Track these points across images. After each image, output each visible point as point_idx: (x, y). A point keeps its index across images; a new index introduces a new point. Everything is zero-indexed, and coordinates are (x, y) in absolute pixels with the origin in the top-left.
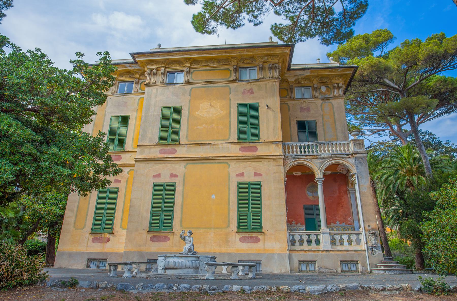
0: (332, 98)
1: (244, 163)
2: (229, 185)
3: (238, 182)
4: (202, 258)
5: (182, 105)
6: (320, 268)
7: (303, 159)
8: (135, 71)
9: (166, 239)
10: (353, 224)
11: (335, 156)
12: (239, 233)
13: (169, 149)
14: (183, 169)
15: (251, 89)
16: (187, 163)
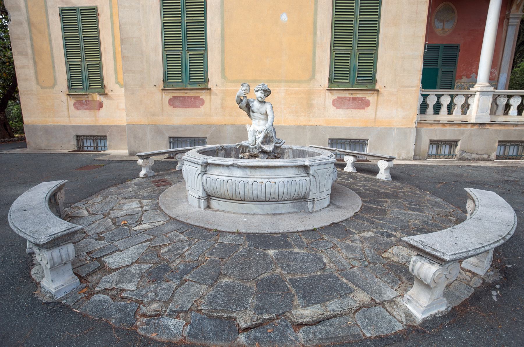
4: (316, 168)
6: (463, 151)
9: (196, 102)
10: (496, 79)
12: (332, 91)
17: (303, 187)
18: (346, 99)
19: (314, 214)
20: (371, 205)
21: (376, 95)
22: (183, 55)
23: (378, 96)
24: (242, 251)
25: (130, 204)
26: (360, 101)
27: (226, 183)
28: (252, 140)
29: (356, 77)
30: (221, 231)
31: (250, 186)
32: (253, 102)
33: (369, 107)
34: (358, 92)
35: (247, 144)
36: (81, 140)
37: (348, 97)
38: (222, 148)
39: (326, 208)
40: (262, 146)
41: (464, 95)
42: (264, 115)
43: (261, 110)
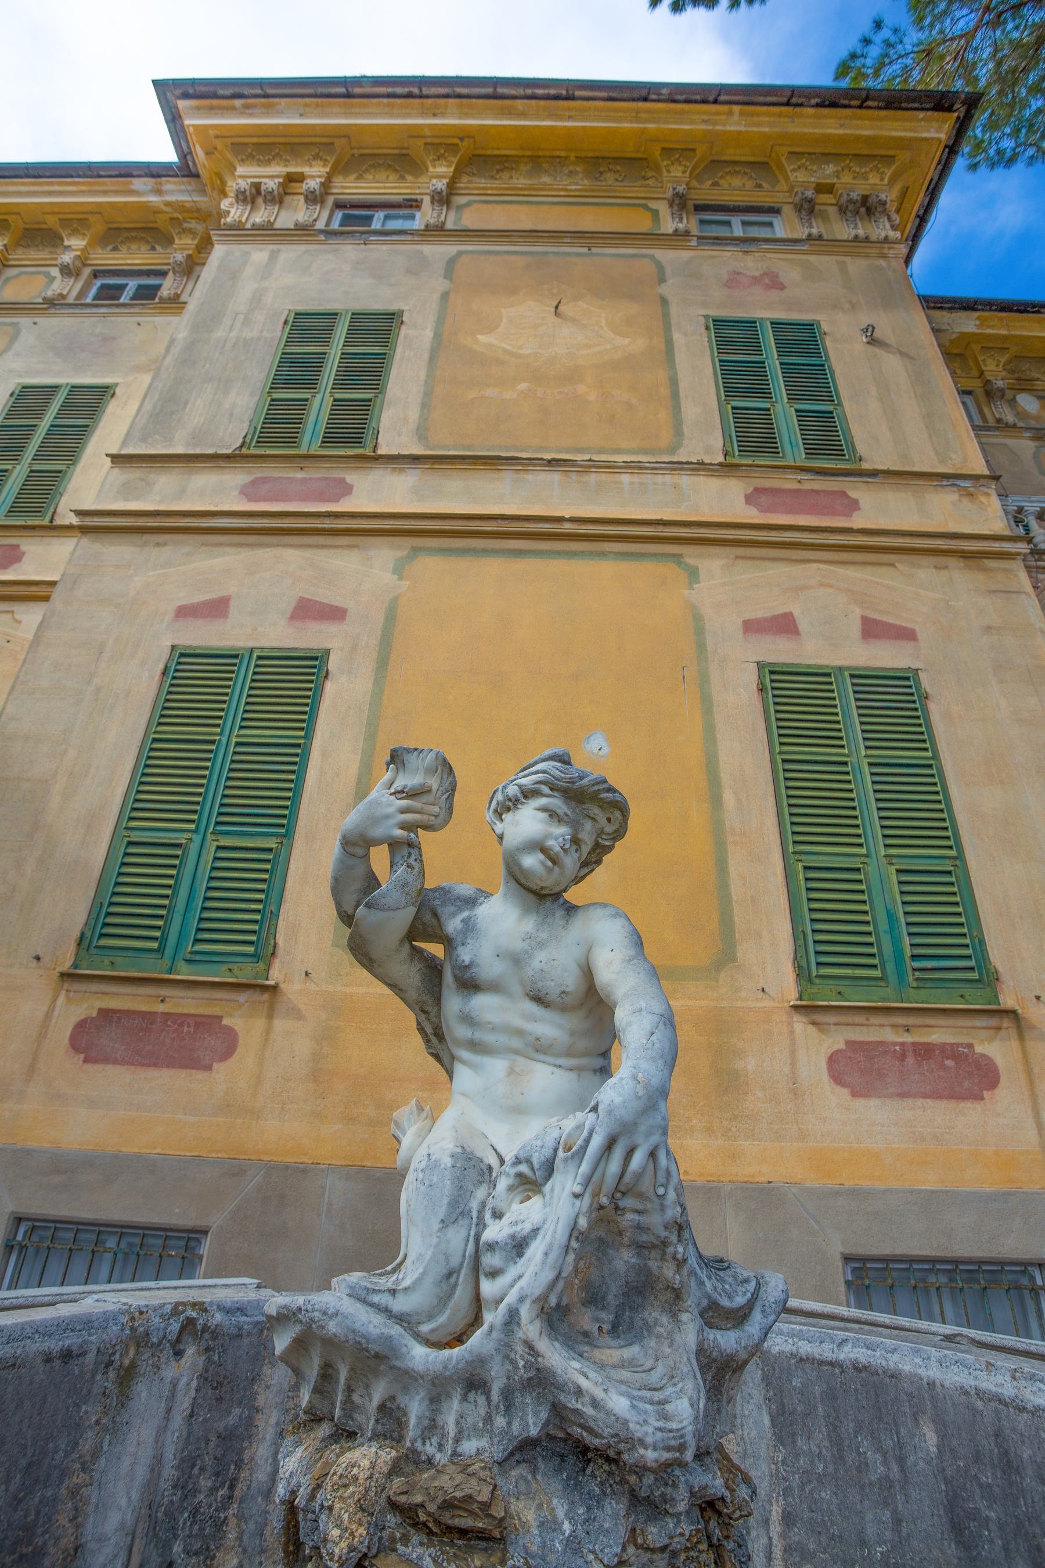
1: (783, 568)
2: (704, 680)
3: (760, 665)
5: (405, 308)
12: (819, 1017)
13: (304, 480)
15: (765, 274)
16: (415, 550)
18: (885, 1053)
21: (1013, 1032)
23: (1021, 1038)
26: (949, 1063)
28: (442, 1270)
29: (908, 960)
32: (471, 902)
33: (997, 1091)
34: (931, 1021)
37: (895, 1044)
38: (191, 1322)
42: (563, 1009)
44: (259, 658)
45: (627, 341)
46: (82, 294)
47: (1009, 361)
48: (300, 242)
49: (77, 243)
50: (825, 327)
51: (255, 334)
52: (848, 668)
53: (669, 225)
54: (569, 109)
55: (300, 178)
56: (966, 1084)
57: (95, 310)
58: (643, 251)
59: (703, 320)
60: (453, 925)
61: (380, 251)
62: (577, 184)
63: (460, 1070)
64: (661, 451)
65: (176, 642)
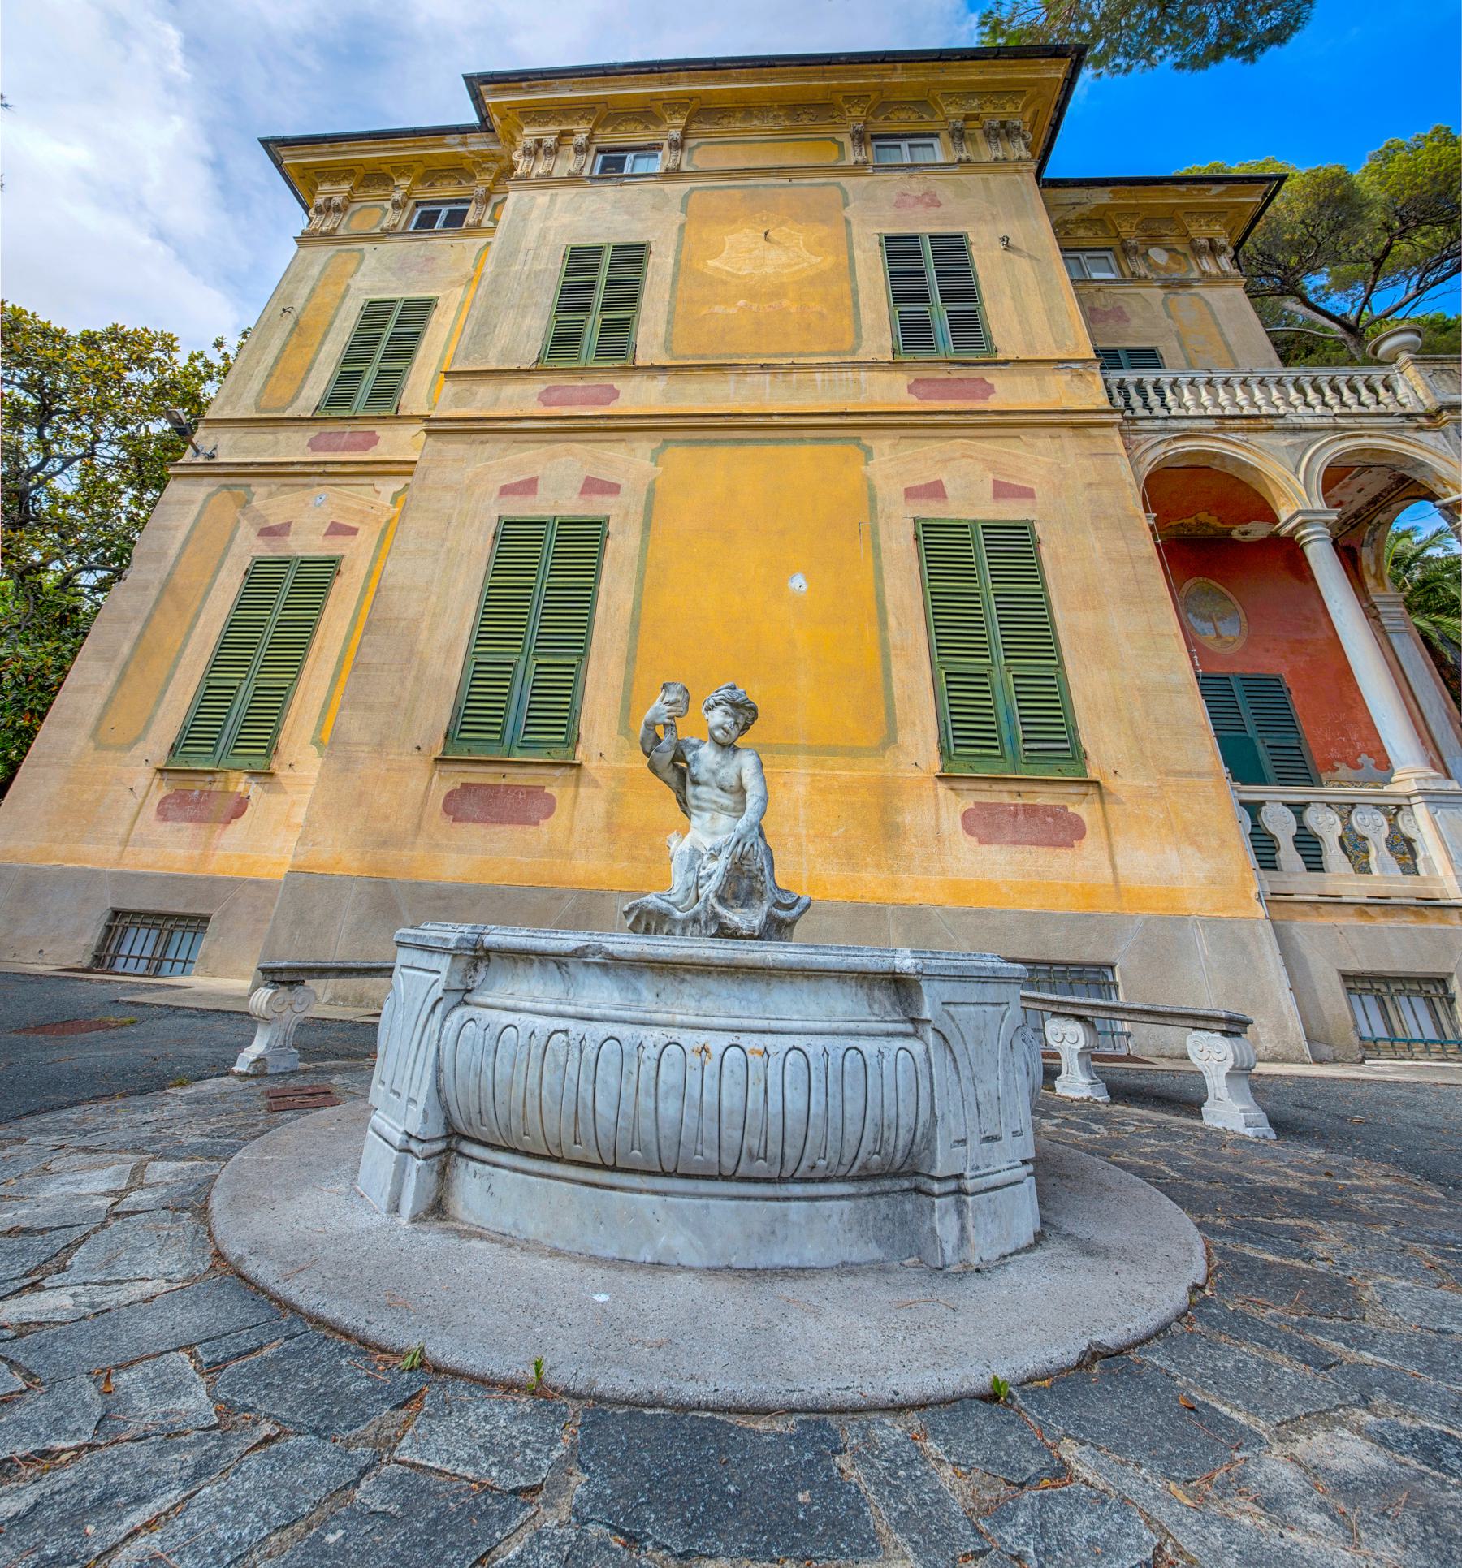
0: (1198, 280)
2: (875, 533)
4: (946, 990)
7: (1207, 431)
8: (480, 161)
11: (1351, 420)
12: (956, 785)
14: (648, 464)
15: (926, 194)
17: (901, 1097)
19: (975, 1283)
20: (1250, 1251)
21: (1096, 797)
22: (521, 666)
23: (1102, 802)
24: (519, 1557)
25: (78, 1177)
26: (1049, 819)
27: (540, 1051)
30: (448, 1371)
31: (648, 1067)
32: (696, 747)
35: (664, 905)
36: (120, 929)
37: (1010, 805)
39: (1028, 1249)
40: (720, 909)
41: (1377, 806)
42: (732, 793)
43: (722, 773)
44: (560, 523)
45: (819, 259)
46: (408, 222)
47: (1142, 222)
48: (573, 186)
49: (404, 183)
50: (972, 238)
51: (542, 267)
52: (981, 521)
53: (851, 157)
54: (771, 74)
55: (572, 134)
56: (1061, 835)
57: (419, 236)
58: (832, 180)
59: (877, 237)
60: (689, 757)
61: (631, 190)
62: (779, 125)
63: (693, 817)
64: (845, 353)
65: (502, 513)
